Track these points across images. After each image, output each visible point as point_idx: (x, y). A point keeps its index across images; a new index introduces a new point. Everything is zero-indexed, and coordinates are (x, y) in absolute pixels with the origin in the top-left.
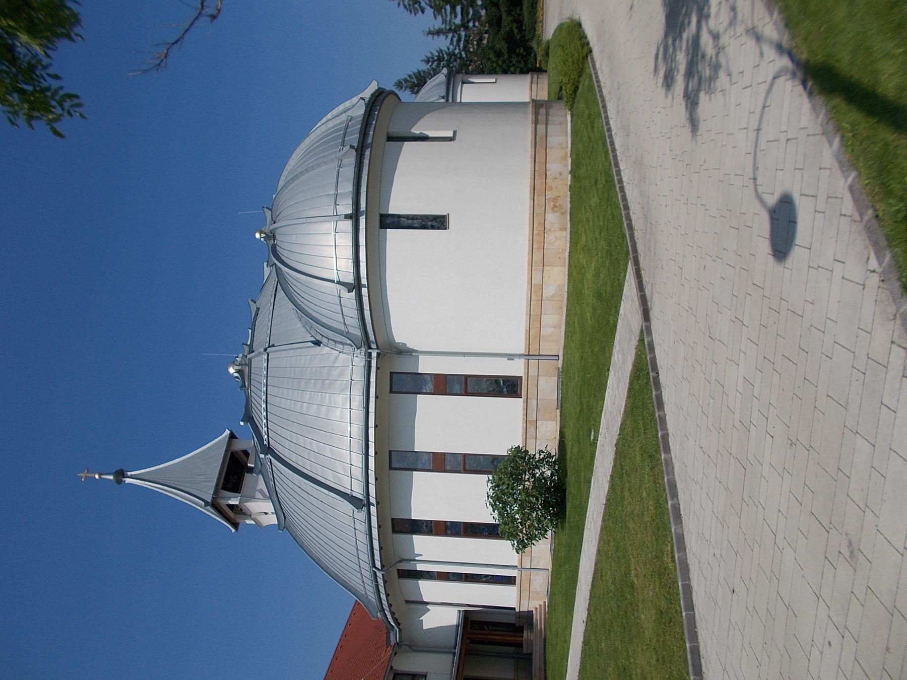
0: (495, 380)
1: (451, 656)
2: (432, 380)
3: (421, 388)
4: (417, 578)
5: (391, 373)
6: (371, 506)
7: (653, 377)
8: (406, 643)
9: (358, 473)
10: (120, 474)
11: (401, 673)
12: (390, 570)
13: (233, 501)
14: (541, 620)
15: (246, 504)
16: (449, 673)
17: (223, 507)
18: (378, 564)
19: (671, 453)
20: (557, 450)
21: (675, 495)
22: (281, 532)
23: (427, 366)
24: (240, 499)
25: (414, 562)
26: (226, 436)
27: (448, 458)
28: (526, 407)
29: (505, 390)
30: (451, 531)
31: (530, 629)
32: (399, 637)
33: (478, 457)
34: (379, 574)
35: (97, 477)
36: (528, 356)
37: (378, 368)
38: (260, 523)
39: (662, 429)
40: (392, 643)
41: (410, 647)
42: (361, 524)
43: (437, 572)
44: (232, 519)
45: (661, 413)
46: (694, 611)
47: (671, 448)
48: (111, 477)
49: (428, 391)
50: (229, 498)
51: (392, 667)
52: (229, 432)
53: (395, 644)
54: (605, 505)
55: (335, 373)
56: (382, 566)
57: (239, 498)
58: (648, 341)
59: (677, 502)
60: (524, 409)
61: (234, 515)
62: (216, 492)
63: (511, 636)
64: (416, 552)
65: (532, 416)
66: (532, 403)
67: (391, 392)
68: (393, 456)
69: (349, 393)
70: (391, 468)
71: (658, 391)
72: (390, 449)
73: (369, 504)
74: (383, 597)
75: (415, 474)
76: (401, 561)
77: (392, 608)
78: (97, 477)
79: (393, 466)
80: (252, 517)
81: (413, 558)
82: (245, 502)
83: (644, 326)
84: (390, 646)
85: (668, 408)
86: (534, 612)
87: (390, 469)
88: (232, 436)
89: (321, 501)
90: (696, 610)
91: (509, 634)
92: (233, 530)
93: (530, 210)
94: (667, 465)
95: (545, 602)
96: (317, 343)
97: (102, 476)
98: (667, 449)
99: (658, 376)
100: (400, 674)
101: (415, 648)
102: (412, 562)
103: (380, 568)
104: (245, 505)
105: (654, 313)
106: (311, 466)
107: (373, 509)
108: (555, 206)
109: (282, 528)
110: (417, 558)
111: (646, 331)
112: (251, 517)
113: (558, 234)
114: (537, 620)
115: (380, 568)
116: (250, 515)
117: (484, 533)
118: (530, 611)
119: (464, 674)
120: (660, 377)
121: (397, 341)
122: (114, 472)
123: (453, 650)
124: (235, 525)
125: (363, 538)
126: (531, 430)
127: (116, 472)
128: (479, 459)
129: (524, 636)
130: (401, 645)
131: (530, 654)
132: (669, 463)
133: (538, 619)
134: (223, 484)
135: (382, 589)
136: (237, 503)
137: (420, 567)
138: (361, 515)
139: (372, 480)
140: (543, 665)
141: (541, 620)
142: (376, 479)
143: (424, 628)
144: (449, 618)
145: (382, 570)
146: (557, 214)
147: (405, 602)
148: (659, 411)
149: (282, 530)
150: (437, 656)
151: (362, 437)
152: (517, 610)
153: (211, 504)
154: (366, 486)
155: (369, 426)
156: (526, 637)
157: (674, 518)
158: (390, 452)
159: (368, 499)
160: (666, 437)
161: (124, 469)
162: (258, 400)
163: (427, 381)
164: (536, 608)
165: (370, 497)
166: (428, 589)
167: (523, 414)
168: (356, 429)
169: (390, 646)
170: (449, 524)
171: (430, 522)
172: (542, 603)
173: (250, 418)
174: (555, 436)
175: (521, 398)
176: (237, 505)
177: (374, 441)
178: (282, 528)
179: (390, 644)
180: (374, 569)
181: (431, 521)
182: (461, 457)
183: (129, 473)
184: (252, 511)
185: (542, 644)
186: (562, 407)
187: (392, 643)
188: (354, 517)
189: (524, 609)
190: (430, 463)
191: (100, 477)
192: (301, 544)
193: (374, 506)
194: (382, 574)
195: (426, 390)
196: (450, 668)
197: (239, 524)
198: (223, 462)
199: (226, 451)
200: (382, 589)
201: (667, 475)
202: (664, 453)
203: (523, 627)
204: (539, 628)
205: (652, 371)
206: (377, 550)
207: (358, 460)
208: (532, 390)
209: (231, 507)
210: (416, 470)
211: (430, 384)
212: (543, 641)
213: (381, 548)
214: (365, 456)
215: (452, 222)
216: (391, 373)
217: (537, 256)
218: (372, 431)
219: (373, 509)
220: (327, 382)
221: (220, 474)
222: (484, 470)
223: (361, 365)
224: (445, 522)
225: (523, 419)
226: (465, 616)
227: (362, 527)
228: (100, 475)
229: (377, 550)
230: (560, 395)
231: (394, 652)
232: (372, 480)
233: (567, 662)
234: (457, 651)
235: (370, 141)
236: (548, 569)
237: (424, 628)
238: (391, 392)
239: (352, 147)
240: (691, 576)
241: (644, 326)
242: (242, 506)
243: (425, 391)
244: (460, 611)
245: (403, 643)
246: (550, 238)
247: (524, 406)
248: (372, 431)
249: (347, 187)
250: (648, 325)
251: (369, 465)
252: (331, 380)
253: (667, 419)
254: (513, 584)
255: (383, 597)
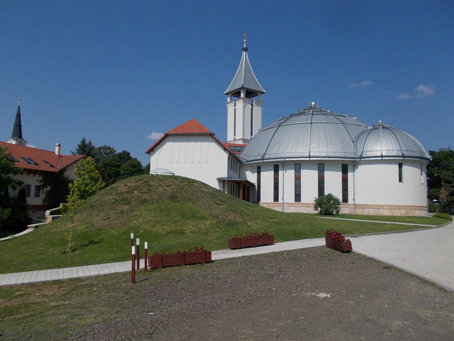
10: (246, 50)
23: (350, 175)
35: (245, 40)
36: (283, 203)
37: (351, 161)
48: (245, 46)
64: (287, 171)
78: (245, 40)
85: (422, 231)
88: (263, 93)
96: (353, 142)
97: (245, 43)
108: (407, 212)
113: (399, 213)
121: (359, 166)
146: (405, 213)
147: (259, 165)
175: (295, 202)
183: (247, 53)
191: (244, 42)
208: (275, 205)
215: (401, 183)
217: (392, 207)
228: (246, 42)
235: (423, 160)
239: (422, 155)
246: (398, 211)
249: (410, 154)
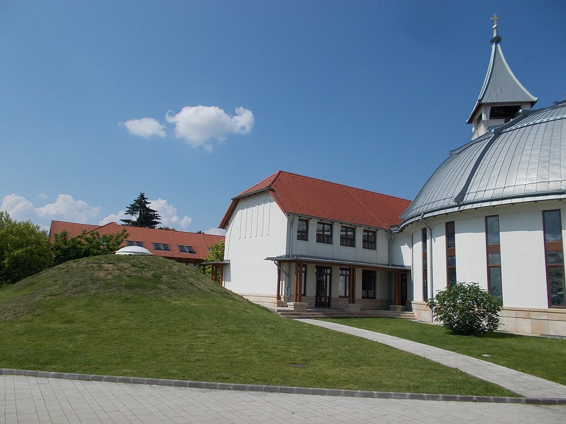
0: (563, 288)
1: (387, 263)
2: (557, 240)
3: (549, 233)
4: (423, 239)
5: (559, 210)
6: (458, 208)
7: (472, 398)
8: (392, 237)
9: (480, 196)
10: (497, 40)
11: (376, 235)
12: (423, 223)
13: (484, 116)
14: (406, 316)
15: (483, 124)
16: (378, 262)
17: (479, 112)
18: (425, 216)
19: (409, 399)
20: (509, 332)
21: (380, 396)
22: (448, 153)
24: (486, 121)
25: (430, 238)
26: (532, 99)
27: (496, 255)
28: (540, 311)
29: (554, 295)
30: (450, 260)
31: (403, 310)
32: (395, 232)
33: (500, 277)
34: (420, 218)
38: (473, 137)
39: (428, 396)
40: (392, 229)
41: (391, 239)
42: (447, 203)
43: (427, 252)
44: (474, 118)
45: (441, 398)
46: (311, 394)
47: (412, 400)
49: (547, 239)
50: (486, 114)
51: (378, 230)
52: (536, 100)
53: (391, 230)
54: (425, 358)
55: (555, 169)
56: (425, 219)
57: (487, 119)
58: (506, 399)
59: (375, 397)
60: (538, 309)
61: (475, 119)
62: (488, 104)
63: (398, 298)
64: (436, 238)
65: (533, 315)
66: (545, 316)
67: (544, 212)
68: (495, 218)
69: (538, 182)
70: (486, 217)
71: (459, 399)
72: (499, 216)
73: (460, 206)
74: (410, 221)
75: (542, 232)
76: (430, 229)
77: (406, 227)
78: (494, 26)
79: (488, 218)
80: (475, 131)
81: (433, 237)
82: (484, 125)
83: (523, 398)
84: (390, 228)
86: (411, 312)
87: (486, 216)
89: (462, 175)
90: (311, 395)
91: (400, 296)
92: (467, 121)
93: (522, 308)
94: (401, 395)
95: (416, 319)
98: (412, 397)
99: (473, 401)
100: (375, 235)
101: (390, 242)
102: (430, 236)
103: (423, 217)
104: (482, 124)
105: (531, 408)
106: (485, 164)
107: (456, 209)
109: (450, 153)
110: (433, 239)
111: (516, 398)
112: (476, 130)
114: (406, 313)
115: (423, 217)
116: (476, 130)
117: (451, 281)
118: (412, 310)
119: (377, 271)
120: (472, 403)
122: (499, 35)
123: (390, 265)
124: (470, 121)
125: (440, 204)
126: (522, 314)
127: (499, 37)
128: (498, 277)
129: (350, 304)
130: (391, 234)
131: (389, 309)
132: (403, 397)
133: (407, 315)
134: (497, 107)
135: (413, 220)
136: (483, 119)
137: (428, 241)
138: (453, 203)
139: (475, 206)
140: (380, 316)
141: (406, 316)
142: (476, 208)
143: (401, 246)
144: (407, 263)
145: (422, 219)
148: (443, 397)
149: (449, 154)
150: (387, 255)
151: (505, 195)
152: (412, 302)
153: (480, 103)
154: (471, 202)
155: (513, 199)
156: (398, 307)
157: (365, 393)
158: (498, 216)
159: (462, 205)
160: (422, 398)
161: (501, 41)
162: (544, 117)
163: (556, 237)
164: (413, 314)
165: (481, 203)
166: (418, 246)
167: (534, 309)
168: (510, 191)
169: (390, 228)
170: (454, 258)
171: (454, 246)
172: (416, 317)
173: (526, 115)
174: (519, 331)
175: (549, 308)
176: (482, 119)
177: (501, 204)
178: (450, 153)
179: (392, 228)
180: (423, 214)
181: (455, 247)
182: (498, 264)
183: (499, 45)
184: (479, 130)
185: (392, 316)
186: (542, 338)
187: (392, 229)
188: (452, 197)
189: (413, 306)
190: (492, 243)
192: (440, 167)
193: (458, 209)
194: (420, 219)
195: (547, 237)
196: (382, 263)
197: (472, 123)
198: (511, 103)
199: (520, 102)
200: (413, 220)
201: (394, 394)
202: (410, 395)
203: (405, 305)
204: (401, 315)
205: (478, 398)
206: (445, 212)
207: (488, 195)
208: (555, 316)
209: (481, 116)
210: (487, 234)
211: (553, 239)
212: (394, 317)
213: (435, 216)
214: (490, 199)
216: (559, 210)
218: (509, 201)
219: (456, 209)
220: (548, 164)
221: (502, 103)
222: (491, 280)
223: (562, 187)
224: (455, 256)
225: (530, 309)
226: (408, 270)
227: (446, 204)
229: (445, 212)
230: (550, 337)
231: (386, 230)
232: (475, 206)
233: (364, 329)
234: (390, 267)
236: (433, 322)
237: (401, 246)
238: (544, 212)
240: (330, 397)
241: (523, 398)
242: (482, 122)
243: (547, 236)
244: (411, 267)
245: (392, 235)
247: (542, 309)
248: (509, 201)
250: (522, 402)
251: (485, 203)
252: (549, 167)
253: (435, 401)
254: (424, 300)
255: (410, 221)
